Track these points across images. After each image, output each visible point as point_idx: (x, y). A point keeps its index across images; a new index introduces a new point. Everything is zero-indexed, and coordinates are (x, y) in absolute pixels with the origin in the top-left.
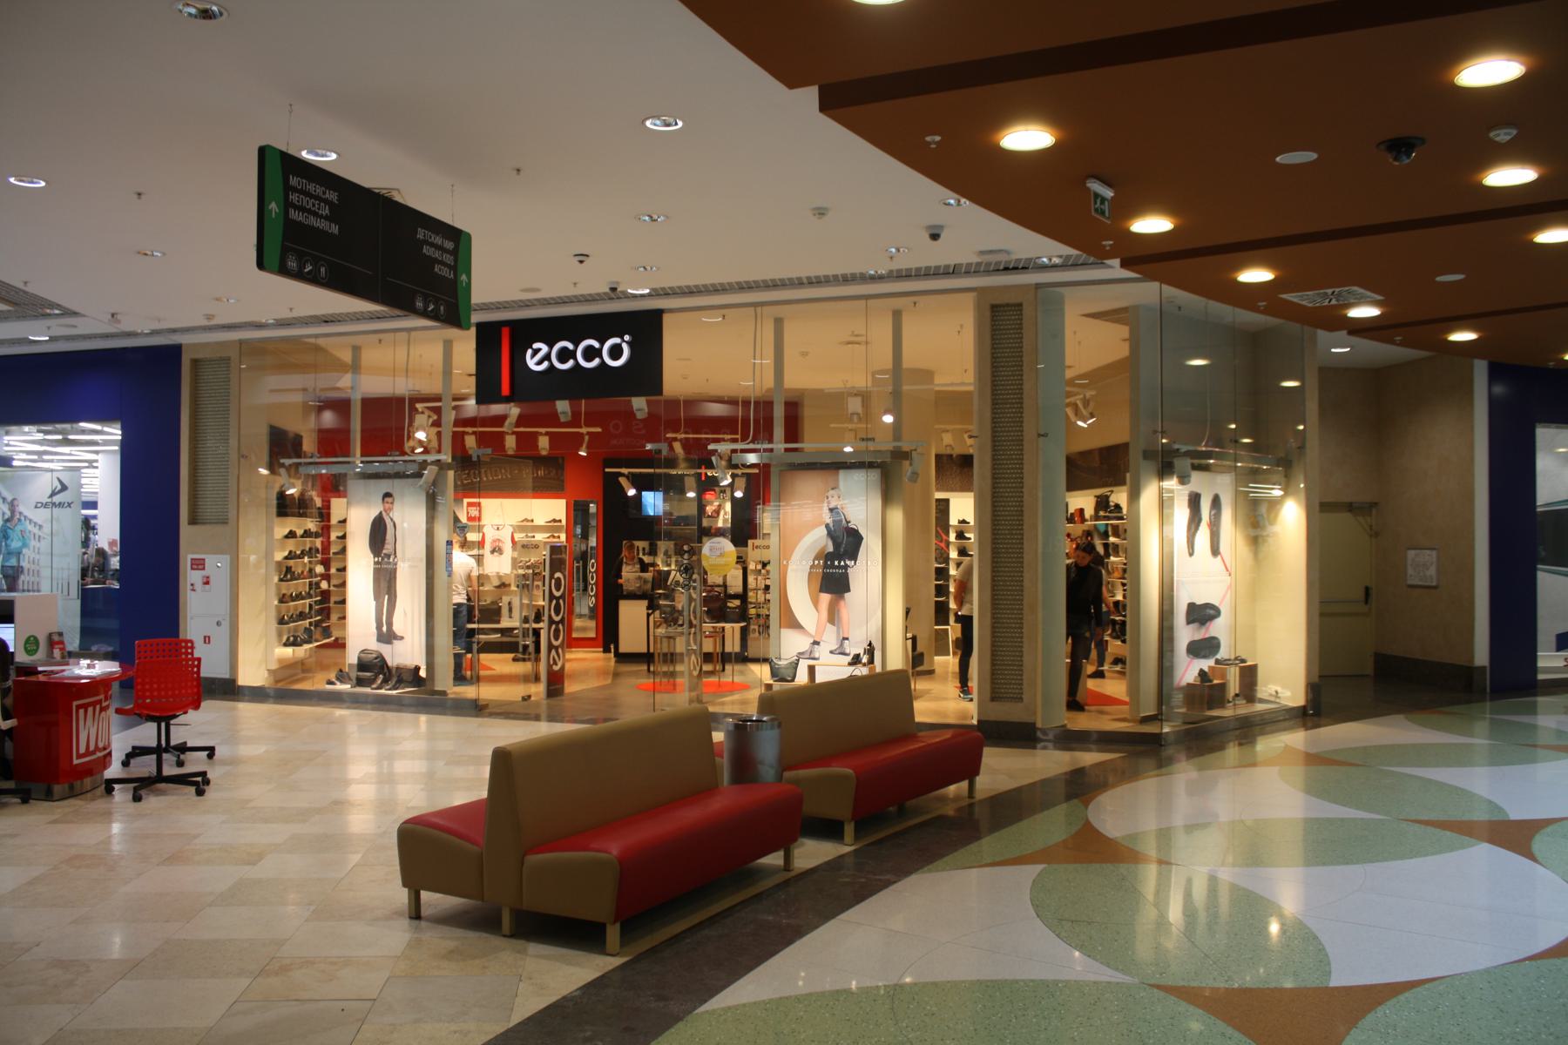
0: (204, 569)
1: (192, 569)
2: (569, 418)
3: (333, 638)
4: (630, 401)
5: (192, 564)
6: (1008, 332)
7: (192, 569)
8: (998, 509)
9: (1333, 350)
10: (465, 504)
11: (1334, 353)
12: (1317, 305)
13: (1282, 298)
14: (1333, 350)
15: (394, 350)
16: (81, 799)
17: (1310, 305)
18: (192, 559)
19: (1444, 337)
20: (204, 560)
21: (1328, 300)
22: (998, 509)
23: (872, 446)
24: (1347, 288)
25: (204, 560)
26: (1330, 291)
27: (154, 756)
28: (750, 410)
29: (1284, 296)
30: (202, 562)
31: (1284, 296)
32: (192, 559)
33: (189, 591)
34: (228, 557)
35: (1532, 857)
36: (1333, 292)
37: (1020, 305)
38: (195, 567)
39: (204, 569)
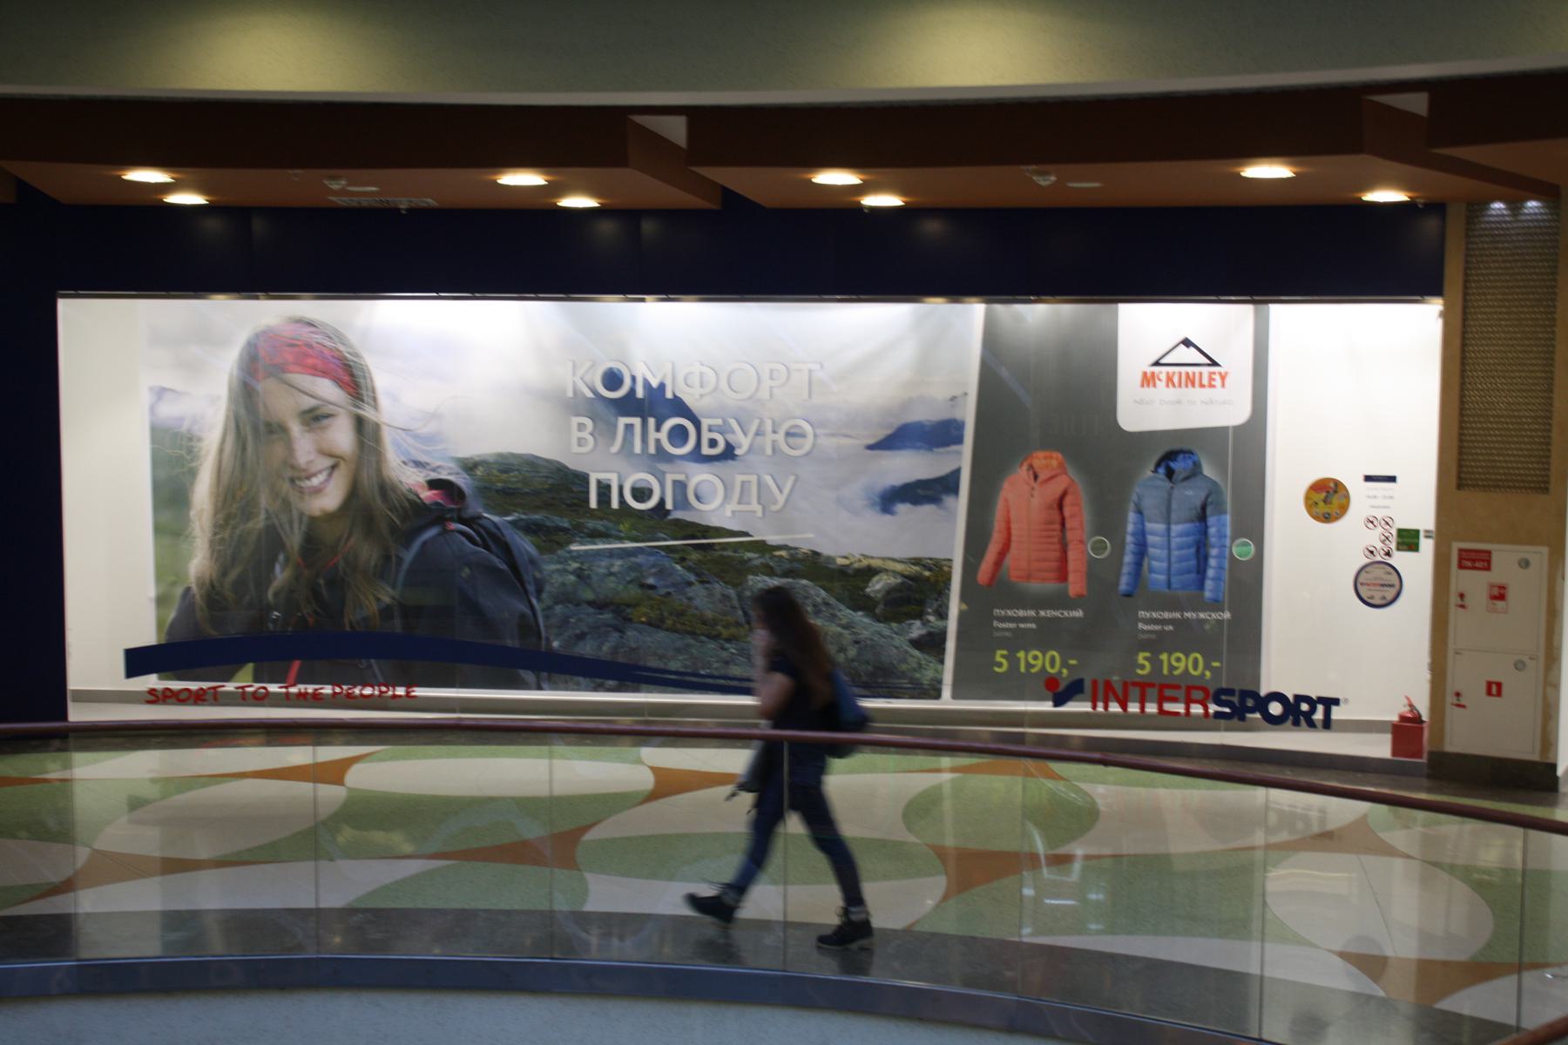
0: (1488, 568)
1: (1461, 567)
4: (1395, 753)
5: (1461, 559)
6: (1517, 459)
7: (1461, 567)
8: (1473, 240)
10: (1425, 755)
15: (551, 781)
16: (371, 761)
18: (1461, 551)
20: (1489, 553)
22: (1473, 240)
25: (1489, 553)
28: (689, 722)
30: (1483, 556)
32: (1461, 551)
33: (1452, 608)
34: (1545, 550)
37: (1546, 490)
38: (1469, 564)
39: (1488, 568)
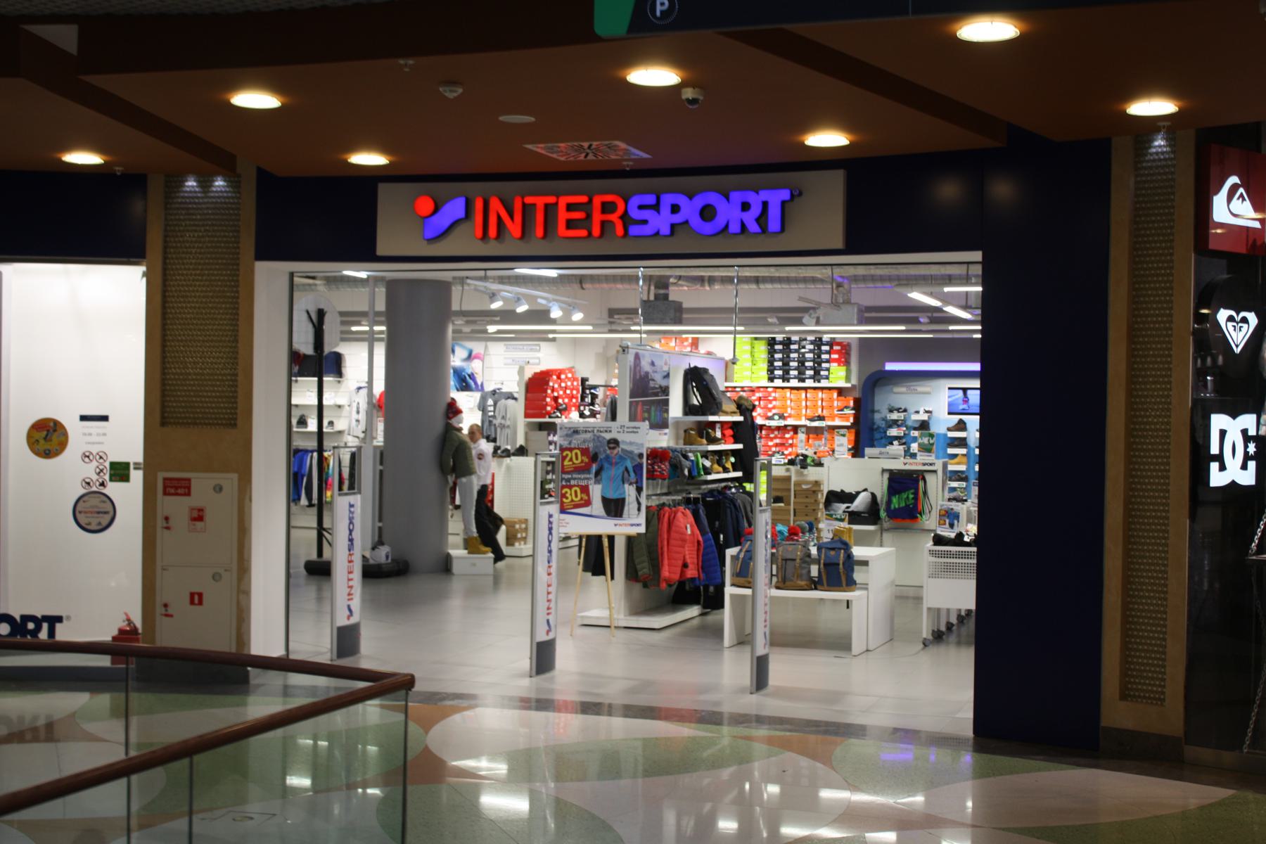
0: (189, 494)
1: (165, 493)
2: (799, 429)
3: (457, 552)
5: (165, 487)
7: (165, 493)
9: (529, 119)
11: (531, 116)
12: (572, 159)
13: (526, 148)
14: (529, 119)
17: (562, 159)
18: (165, 479)
19: (59, 155)
20: (189, 480)
21: (583, 155)
23: (476, 461)
24: (607, 142)
25: (189, 480)
26: (586, 145)
27: (733, 336)
29: (530, 146)
31: (530, 146)
32: (165, 479)
35: (832, 768)
36: (591, 145)
38: (172, 491)
39: (189, 494)
